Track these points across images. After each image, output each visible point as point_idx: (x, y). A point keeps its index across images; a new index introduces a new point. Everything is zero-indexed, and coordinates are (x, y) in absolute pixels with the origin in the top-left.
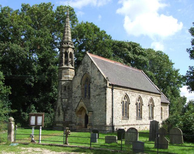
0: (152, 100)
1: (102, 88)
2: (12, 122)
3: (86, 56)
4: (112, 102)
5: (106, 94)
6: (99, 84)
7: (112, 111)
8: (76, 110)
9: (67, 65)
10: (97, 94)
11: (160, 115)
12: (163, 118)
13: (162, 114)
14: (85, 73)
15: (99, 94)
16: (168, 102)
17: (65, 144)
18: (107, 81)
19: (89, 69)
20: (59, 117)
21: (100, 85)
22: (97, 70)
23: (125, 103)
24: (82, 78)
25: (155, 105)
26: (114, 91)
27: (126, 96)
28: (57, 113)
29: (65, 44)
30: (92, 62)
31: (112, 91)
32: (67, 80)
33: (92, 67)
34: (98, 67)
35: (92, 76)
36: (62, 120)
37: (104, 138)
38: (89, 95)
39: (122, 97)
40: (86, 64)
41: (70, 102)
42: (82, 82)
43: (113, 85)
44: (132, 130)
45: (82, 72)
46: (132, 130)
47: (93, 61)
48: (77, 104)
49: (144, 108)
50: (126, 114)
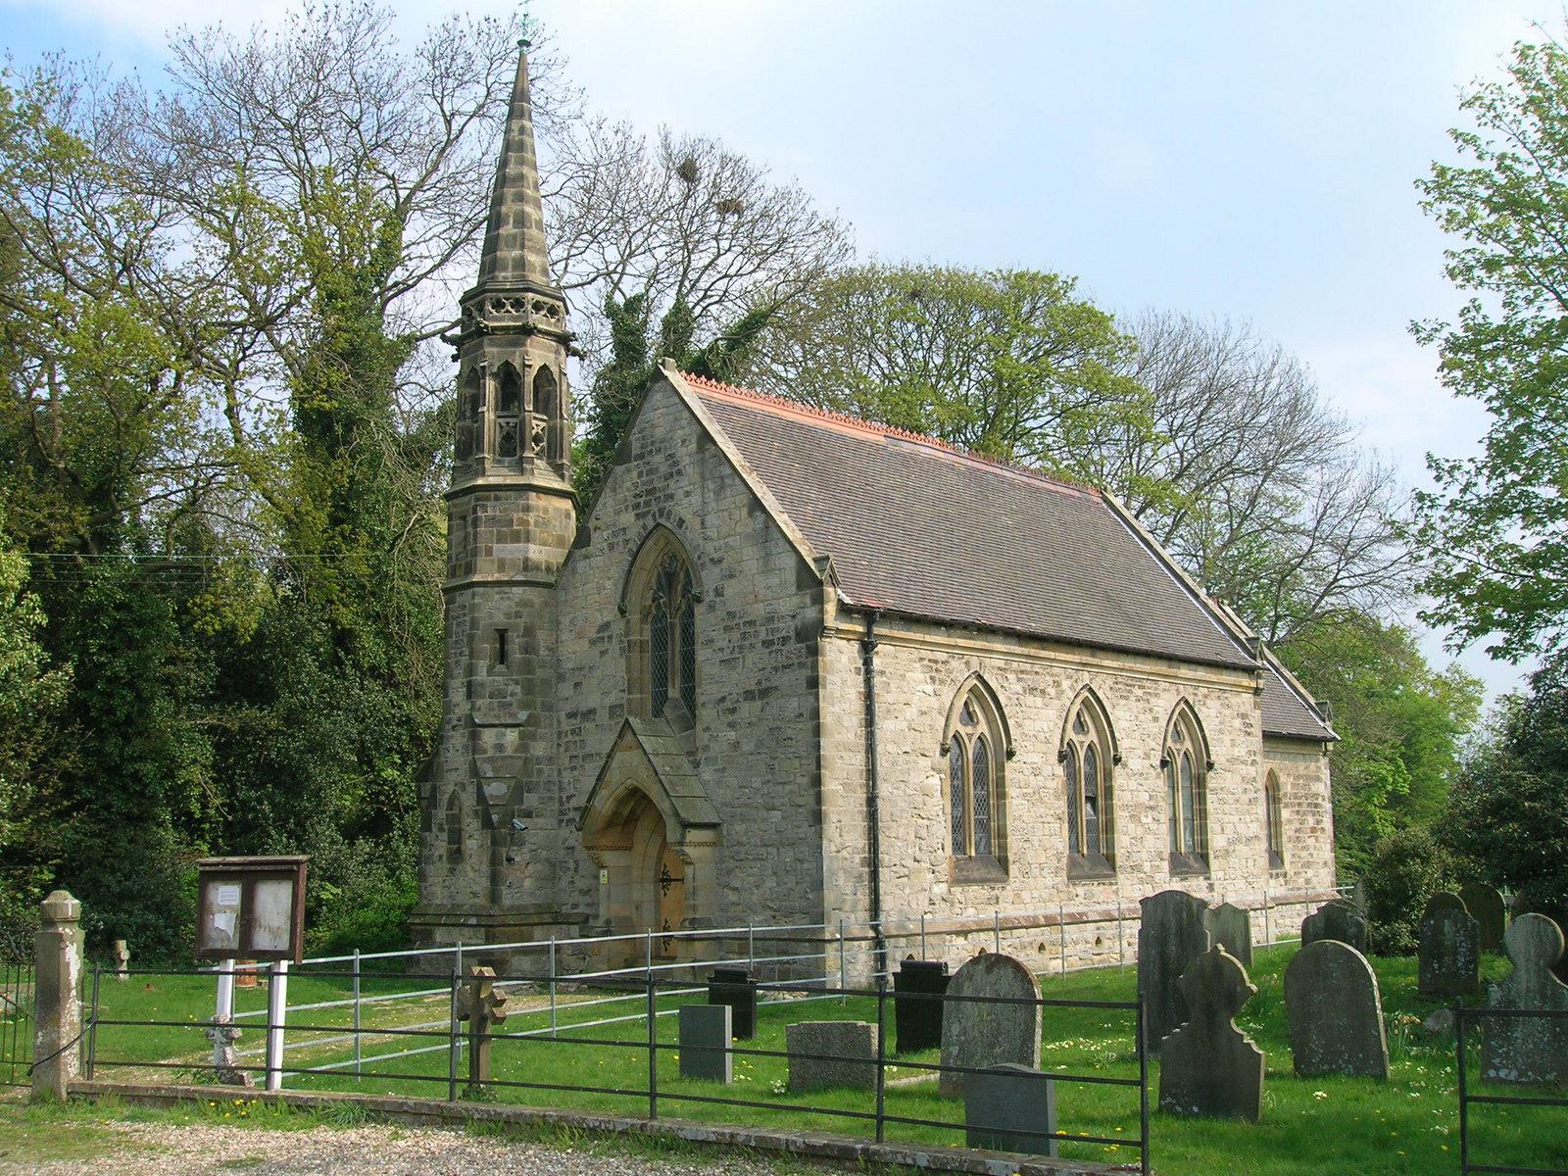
0: (1187, 719)
1: (785, 640)
2: (67, 930)
3: (658, 396)
4: (870, 749)
5: (814, 683)
6: (759, 610)
7: (872, 816)
8: (585, 811)
9: (520, 466)
10: (752, 686)
11: (1263, 834)
12: (1287, 857)
13: (1273, 825)
14: (651, 524)
15: (765, 684)
16: (1320, 734)
17: (466, 1095)
18: (821, 583)
19: (688, 494)
20: (452, 871)
21: (770, 619)
22: (744, 499)
23: (971, 748)
24: (632, 564)
25: (1218, 753)
26: (877, 663)
28: (441, 846)
29: (498, 305)
30: (705, 437)
31: (867, 662)
33: (703, 478)
34: (752, 480)
35: (710, 547)
36: (482, 901)
37: (780, 1045)
38: (689, 694)
40: (658, 459)
42: (634, 597)
43: (869, 615)
44: (989, 970)
45: (628, 518)
46: (989, 970)
47: (713, 429)
48: (593, 768)
49: (1133, 785)
50: (981, 844)
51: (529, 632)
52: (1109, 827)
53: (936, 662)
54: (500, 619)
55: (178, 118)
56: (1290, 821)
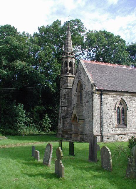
26: (103, 97)
27: (122, 102)
30: (83, 68)
31: (101, 97)
32: (66, 89)
34: (88, 74)
35: (84, 82)
39: (116, 101)
41: (69, 109)
51: (68, 95)
53: (114, 97)
54: (65, 93)
55: (125, 45)
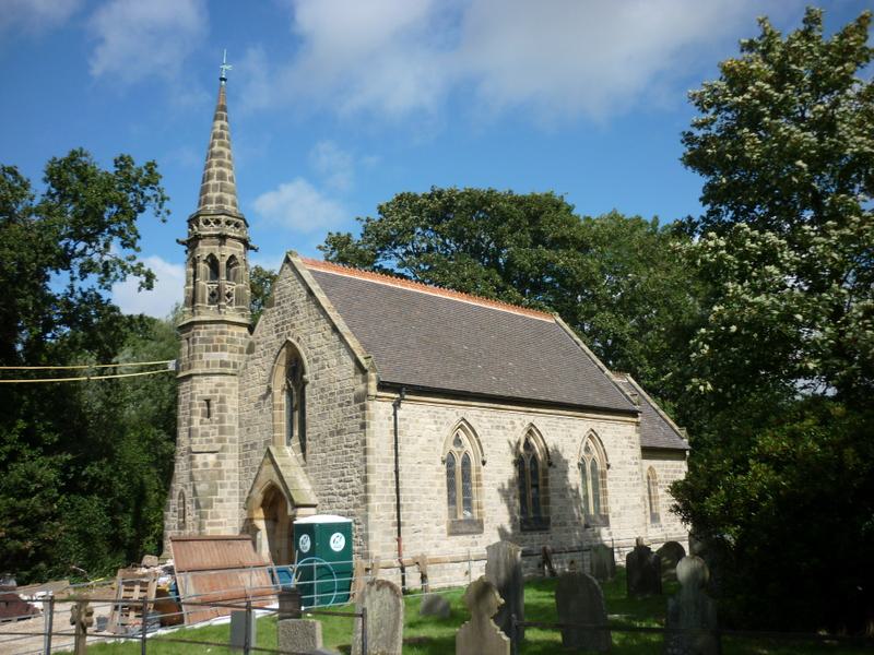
51: (222, 400)
52: (547, 501)
56: (663, 496)
